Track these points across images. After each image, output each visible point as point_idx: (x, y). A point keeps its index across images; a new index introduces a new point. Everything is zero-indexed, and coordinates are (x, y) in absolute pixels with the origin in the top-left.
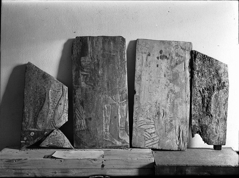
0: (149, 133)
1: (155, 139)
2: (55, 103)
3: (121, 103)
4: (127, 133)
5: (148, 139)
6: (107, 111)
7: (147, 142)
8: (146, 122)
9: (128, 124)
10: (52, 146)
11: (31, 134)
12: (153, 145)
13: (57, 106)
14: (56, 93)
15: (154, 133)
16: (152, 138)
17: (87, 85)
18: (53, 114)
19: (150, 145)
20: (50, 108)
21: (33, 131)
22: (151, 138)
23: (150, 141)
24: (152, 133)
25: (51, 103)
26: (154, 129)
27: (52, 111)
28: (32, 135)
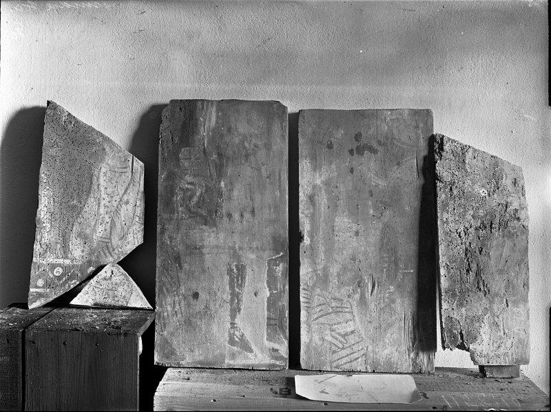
0: (339, 334)
1: (355, 348)
2: (114, 198)
3: (272, 259)
4: (284, 332)
5: (339, 348)
6: (237, 278)
7: (336, 356)
8: (332, 308)
9: (287, 312)
10: (101, 305)
11: (55, 272)
12: (351, 361)
13: (117, 207)
14: (117, 175)
15: (352, 332)
16: (350, 346)
17: (192, 215)
18: (109, 224)
19: (346, 363)
20: (102, 210)
21: (60, 265)
22: (346, 346)
23: (344, 353)
24: (346, 334)
25: (104, 199)
26: (351, 323)
27: (107, 219)
28: (58, 275)
